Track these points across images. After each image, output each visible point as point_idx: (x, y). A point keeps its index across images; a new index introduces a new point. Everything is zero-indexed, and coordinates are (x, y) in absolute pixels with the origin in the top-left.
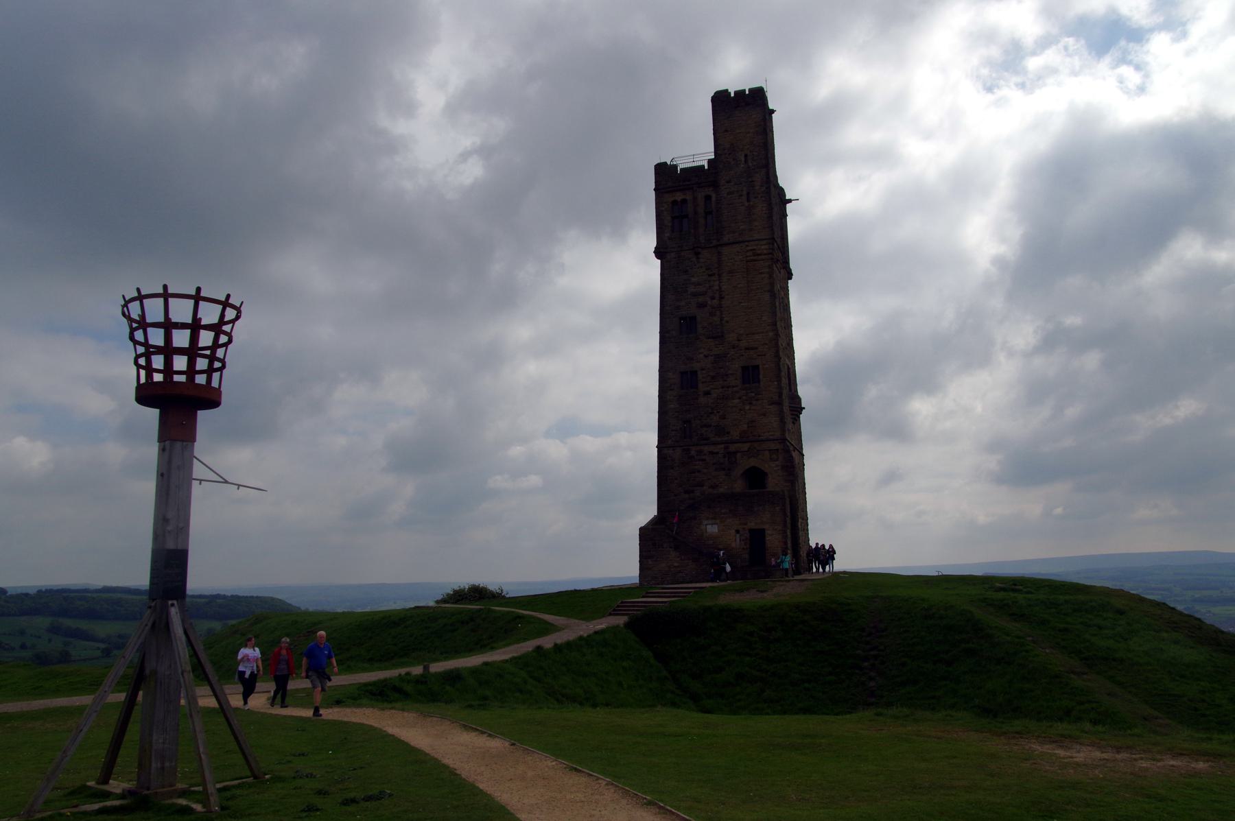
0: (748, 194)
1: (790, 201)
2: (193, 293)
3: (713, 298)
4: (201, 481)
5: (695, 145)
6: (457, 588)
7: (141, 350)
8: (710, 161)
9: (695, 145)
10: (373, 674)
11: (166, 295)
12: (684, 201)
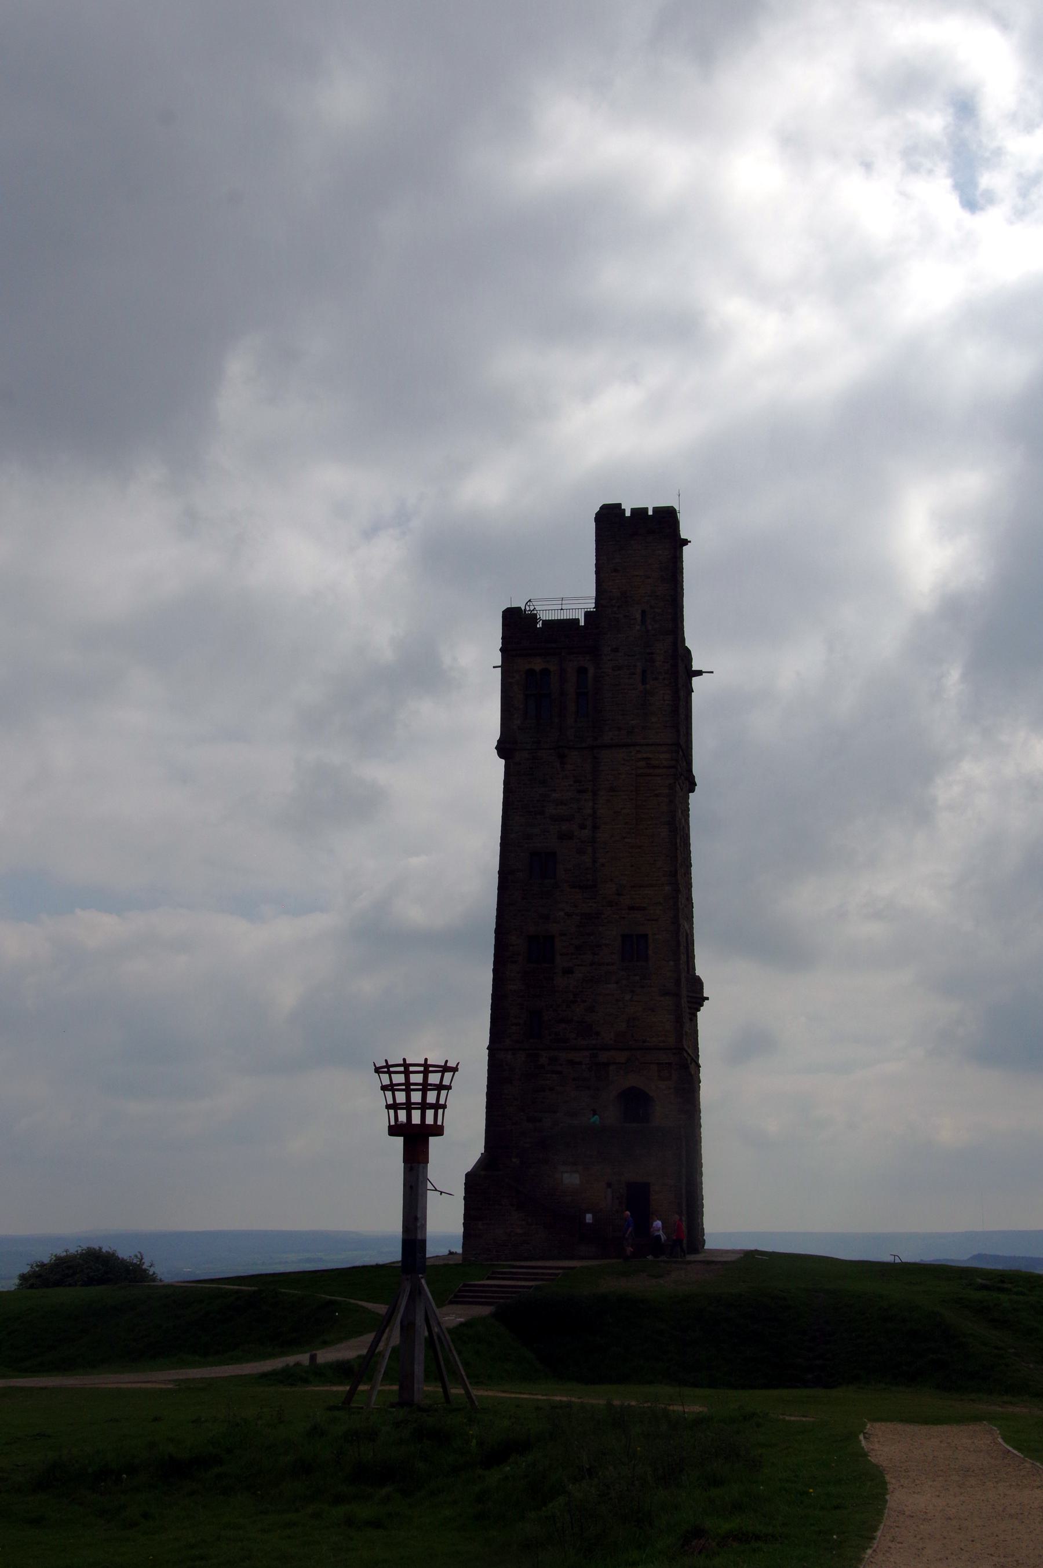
0: (644, 672)
1: (699, 673)
3: (582, 827)
4: (441, 1193)
5: (569, 589)
6: (60, 1252)
9: (569, 589)
10: (12, 1384)
12: (545, 672)
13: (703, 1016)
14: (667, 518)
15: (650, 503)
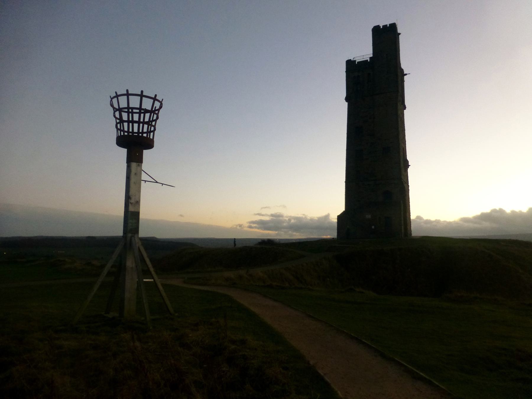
1: (406, 74)
2: (140, 93)
4: (145, 181)
5: (364, 51)
7: (118, 121)
8: (370, 58)
9: (364, 51)
11: (128, 95)
13: (409, 170)
14: (393, 26)
15: (388, 23)
